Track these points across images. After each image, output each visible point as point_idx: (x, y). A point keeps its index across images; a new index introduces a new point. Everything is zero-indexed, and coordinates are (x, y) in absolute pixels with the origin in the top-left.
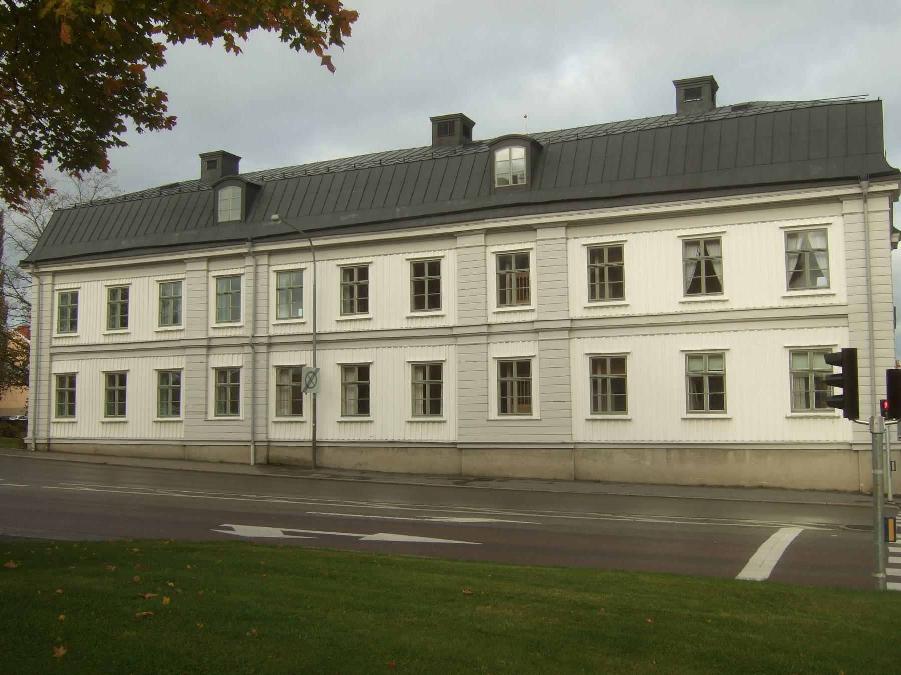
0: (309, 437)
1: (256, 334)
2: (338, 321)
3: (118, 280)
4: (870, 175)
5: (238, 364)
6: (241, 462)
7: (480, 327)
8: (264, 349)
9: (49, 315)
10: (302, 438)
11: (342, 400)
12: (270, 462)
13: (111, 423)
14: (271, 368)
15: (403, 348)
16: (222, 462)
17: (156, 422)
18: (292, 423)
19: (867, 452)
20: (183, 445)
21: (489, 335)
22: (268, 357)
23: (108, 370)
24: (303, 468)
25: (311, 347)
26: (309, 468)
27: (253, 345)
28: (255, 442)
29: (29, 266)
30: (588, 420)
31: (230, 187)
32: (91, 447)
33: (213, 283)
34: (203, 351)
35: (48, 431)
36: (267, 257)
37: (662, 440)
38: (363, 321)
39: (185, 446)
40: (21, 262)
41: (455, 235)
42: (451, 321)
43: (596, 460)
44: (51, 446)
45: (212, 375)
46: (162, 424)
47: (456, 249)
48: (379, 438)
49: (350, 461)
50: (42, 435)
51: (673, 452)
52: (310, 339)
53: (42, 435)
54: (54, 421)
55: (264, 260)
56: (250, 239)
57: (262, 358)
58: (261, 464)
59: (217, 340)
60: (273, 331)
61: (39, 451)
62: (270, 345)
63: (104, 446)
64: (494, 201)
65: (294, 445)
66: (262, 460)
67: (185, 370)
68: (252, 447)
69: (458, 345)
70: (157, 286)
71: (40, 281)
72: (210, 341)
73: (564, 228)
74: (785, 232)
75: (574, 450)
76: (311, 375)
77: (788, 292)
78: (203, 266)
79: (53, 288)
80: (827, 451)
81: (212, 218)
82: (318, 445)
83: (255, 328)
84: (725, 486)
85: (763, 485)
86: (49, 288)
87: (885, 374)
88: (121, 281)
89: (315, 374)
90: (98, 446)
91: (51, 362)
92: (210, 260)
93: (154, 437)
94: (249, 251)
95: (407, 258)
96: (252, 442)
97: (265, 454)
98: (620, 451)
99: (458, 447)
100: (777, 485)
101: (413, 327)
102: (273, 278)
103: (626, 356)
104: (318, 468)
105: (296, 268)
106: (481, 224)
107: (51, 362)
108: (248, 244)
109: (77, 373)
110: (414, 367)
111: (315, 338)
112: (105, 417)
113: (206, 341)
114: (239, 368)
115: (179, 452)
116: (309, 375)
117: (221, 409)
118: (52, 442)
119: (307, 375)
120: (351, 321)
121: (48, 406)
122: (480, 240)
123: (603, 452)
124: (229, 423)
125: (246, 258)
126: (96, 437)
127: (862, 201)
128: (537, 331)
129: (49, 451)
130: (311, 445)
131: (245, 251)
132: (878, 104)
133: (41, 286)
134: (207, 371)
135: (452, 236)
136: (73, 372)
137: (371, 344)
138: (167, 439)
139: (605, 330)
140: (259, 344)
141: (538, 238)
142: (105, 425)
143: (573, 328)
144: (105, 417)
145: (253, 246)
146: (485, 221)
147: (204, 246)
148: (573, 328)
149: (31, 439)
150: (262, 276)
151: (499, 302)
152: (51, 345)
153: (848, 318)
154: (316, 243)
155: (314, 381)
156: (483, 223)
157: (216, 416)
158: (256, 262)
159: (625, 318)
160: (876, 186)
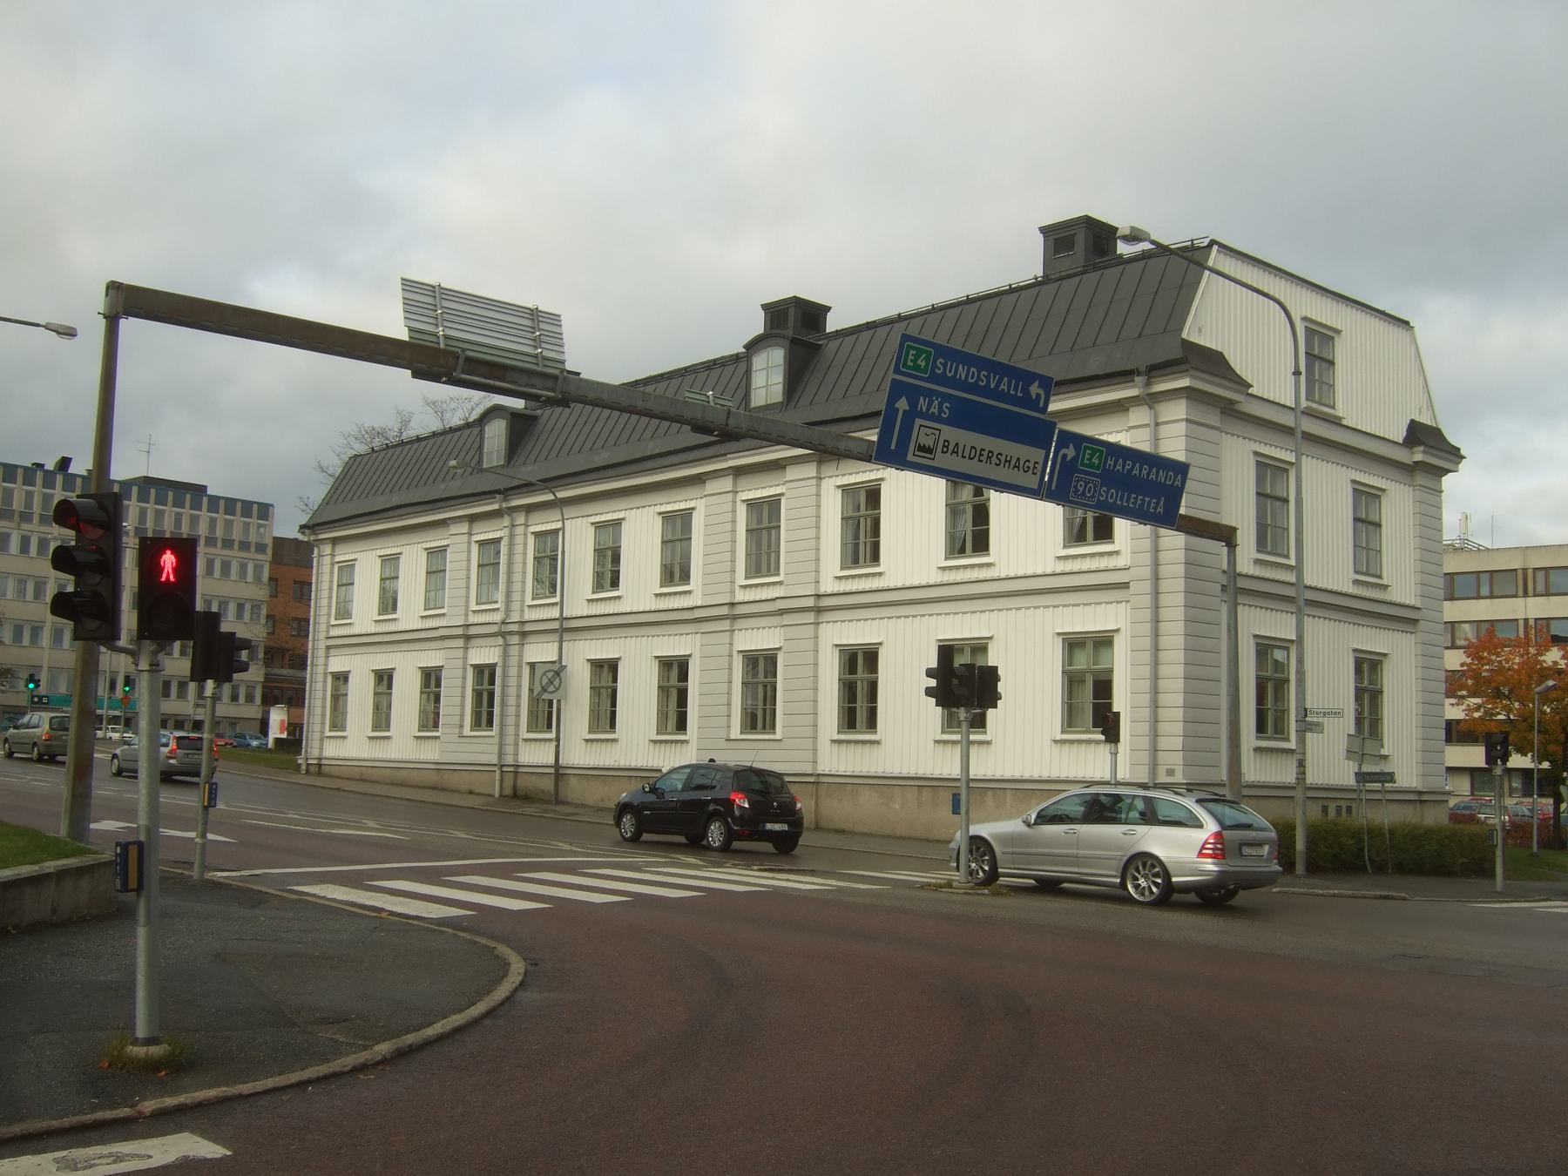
0: (551, 761)
2: (589, 601)
3: (675, 502)
8: (515, 639)
10: (545, 763)
11: (591, 711)
14: (735, 654)
16: (471, 792)
17: (655, 742)
20: (439, 768)
21: (735, 618)
22: (731, 638)
23: (477, 663)
25: (556, 637)
26: (549, 802)
28: (502, 766)
29: (1133, 381)
32: (357, 769)
35: (321, 748)
36: (524, 513)
37: (912, 773)
38: (1079, 559)
40: (302, 527)
42: (696, 600)
44: (323, 767)
47: (706, 496)
48: (623, 763)
50: (315, 753)
51: (925, 789)
52: (556, 625)
55: (520, 519)
56: (1143, 369)
57: (514, 651)
58: (506, 796)
60: (530, 615)
62: (524, 634)
63: (362, 768)
65: (536, 771)
68: (498, 773)
69: (702, 633)
70: (659, 520)
73: (815, 463)
76: (550, 675)
83: (508, 611)
86: (327, 560)
89: (557, 674)
92: (473, 519)
93: (545, 762)
98: (868, 787)
102: (531, 540)
103: (1113, 636)
104: (559, 802)
106: (721, 461)
107: (327, 657)
108: (1138, 379)
109: (690, 656)
114: (494, 665)
115: (432, 778)
117: (477, 724)
118: (324, 762)
119: (544, 674)
120: (544, 605)
122: (726, 483)
123: (849, 788)
125: (1131, 409)
126: (650, 765)
127: (1146, 408)
128: (782, 612)
129: (320, 774)
130: (552, 771)
131: (496, 506)
134: (730, 656)
135: (699, 480)
137: (635, 631)
138: (991, 778)
140: (511, 633)
142: (590, 743)
143: (820, 608)
145: (1148, 384)
146: (729, 456)
148: (820, 608)
150: (519, 539)
153: (1128, 587)
154: (562, 494)
155: (556, 683)
156: (727, 460)
160: (1163, 381)
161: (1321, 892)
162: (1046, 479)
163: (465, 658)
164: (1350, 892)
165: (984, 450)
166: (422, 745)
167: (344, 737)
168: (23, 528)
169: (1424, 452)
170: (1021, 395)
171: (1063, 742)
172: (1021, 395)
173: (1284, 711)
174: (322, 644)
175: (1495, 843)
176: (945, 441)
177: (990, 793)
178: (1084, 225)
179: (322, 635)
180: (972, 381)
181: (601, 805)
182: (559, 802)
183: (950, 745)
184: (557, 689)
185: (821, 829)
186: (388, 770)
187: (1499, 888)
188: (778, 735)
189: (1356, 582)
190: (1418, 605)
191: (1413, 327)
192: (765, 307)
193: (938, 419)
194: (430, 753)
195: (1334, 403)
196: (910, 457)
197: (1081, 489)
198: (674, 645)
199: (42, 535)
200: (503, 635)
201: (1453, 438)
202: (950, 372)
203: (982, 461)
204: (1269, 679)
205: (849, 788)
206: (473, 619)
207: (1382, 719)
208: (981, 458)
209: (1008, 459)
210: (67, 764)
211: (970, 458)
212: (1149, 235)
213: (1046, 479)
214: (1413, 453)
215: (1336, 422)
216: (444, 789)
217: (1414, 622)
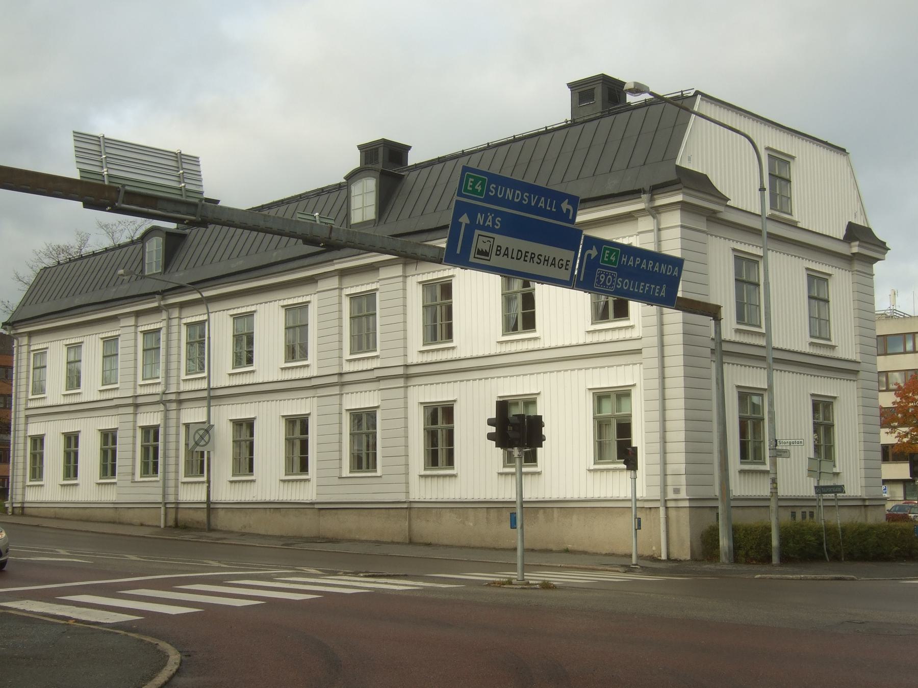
1: (169, 390)
4: (653, 186)
5: (361, 406)
7: (325, 377)
8: (174, 406)
9: (133, 359)
11: (234, 459)
12: (179, 525)
13: (239, 481)
15: (478, 380)
17: (99, 484)
18: (195, 483)
19: (680, 509)
20: (116, 507)
24: (197, 529)
25: (205, 403)
26: (202, 530)
27: (164, 402)
30: (500, 474)
31: (363, 179)
32: (52, 510)
33: (140, 337)
34: (131, 410)
39: (116, 508)
41: (316, 279)
43: (428, 521)
44: (25, 509)
45: (346, 419)
46: (427, 479)
48: (259, 498)
49: (237, 522)
50: (19, 498)
51: (492, 510)
52: (205, 394)
53: (19, 498)
54: (29, 484)
55: (175, 313)
56: (647, 188)
57: (173, 414)
58: (170, 527)
59: (348, 375)
60: (184, 387)
61: (16, 515)
62: (180, 402)
65: (193, 507)
66: (171, 523)
67: (381, 408)
68: (163, 509)
69: (318, 397)
71: (169, 314)
72: (179, 395)
75: (409, 509)
77: (503, 337)
78: (131, 321)
79: (179, 322)
80: (626, 509)
81: (346, 220)
82: (212, 506)
83: (167, 384)
85: (569, 549)
88: (73, 339)
89: (207, 431)
90: (57, 509)
91: (27, 424)
94: (159, 304)
95: (282, 305)
96: (663, 501)
97: (173, 516)
99: (316, 506)
100: (581, 548)
101: (104, 398)
102: (184, 329)
104: (211, 529)
105: (197, 320)
107: (26, 424)
108: (645, 197)
109: (309, 414)
110: (288, 422)
111: (209, 393)
112: (64, 480)
113: (131, 399)
114: (158, 426)
115: (111, 514)
116: (199, 432)
117: (145, 472)
118: (26, 505)
119: (197, 432)
121: (23, 469)
122: (334, 282)
124: (362, 481)
128: (379, 379)
129: (23, 514)
130: (205, 506)
131: (156, 304)
133: (19, 348)
134: (340, 414)
136: (41, 434)
138: (453, 500)
139: (506, 368)
140: (170, 401)
141: (380, 278)
144: (64, 480)
146: (335, 261)
150: (175, 329)
151: (594, 318)
152: (179, 389)
153: (641, 353)
154: (207, 294)
155: (206, 438)
156: (334, 264)
157: (351, 472)
158: (658, 224)
159: (497, 357)
163: (135, 422)
164: (813, 576)
166: (103, 490)
167: (42, 486)
169: (859, 246)
170: (555, 210)
171: (595, 471)
174: (22, 414)
176: (498, 246)
177: (541, 511)
178: (601, 81)
181: (243, 531)
182: (211, 529)
184: (207, 443)
186: (76, 510)
188: (379, 473)
192: (361, 147)
194: (109, 495)
195: (792, 211)
196: (472, 259)
197: (603, 280)
198: (296, 407)
200: (164, 402)
203: (526, 261)
204: (749, 418)
205: (434, 511)
206: (140, 391)
207: (833, 446)
208: (526, 258)
209: (547, 259)
211: (517, 259)
216: (121, 523)
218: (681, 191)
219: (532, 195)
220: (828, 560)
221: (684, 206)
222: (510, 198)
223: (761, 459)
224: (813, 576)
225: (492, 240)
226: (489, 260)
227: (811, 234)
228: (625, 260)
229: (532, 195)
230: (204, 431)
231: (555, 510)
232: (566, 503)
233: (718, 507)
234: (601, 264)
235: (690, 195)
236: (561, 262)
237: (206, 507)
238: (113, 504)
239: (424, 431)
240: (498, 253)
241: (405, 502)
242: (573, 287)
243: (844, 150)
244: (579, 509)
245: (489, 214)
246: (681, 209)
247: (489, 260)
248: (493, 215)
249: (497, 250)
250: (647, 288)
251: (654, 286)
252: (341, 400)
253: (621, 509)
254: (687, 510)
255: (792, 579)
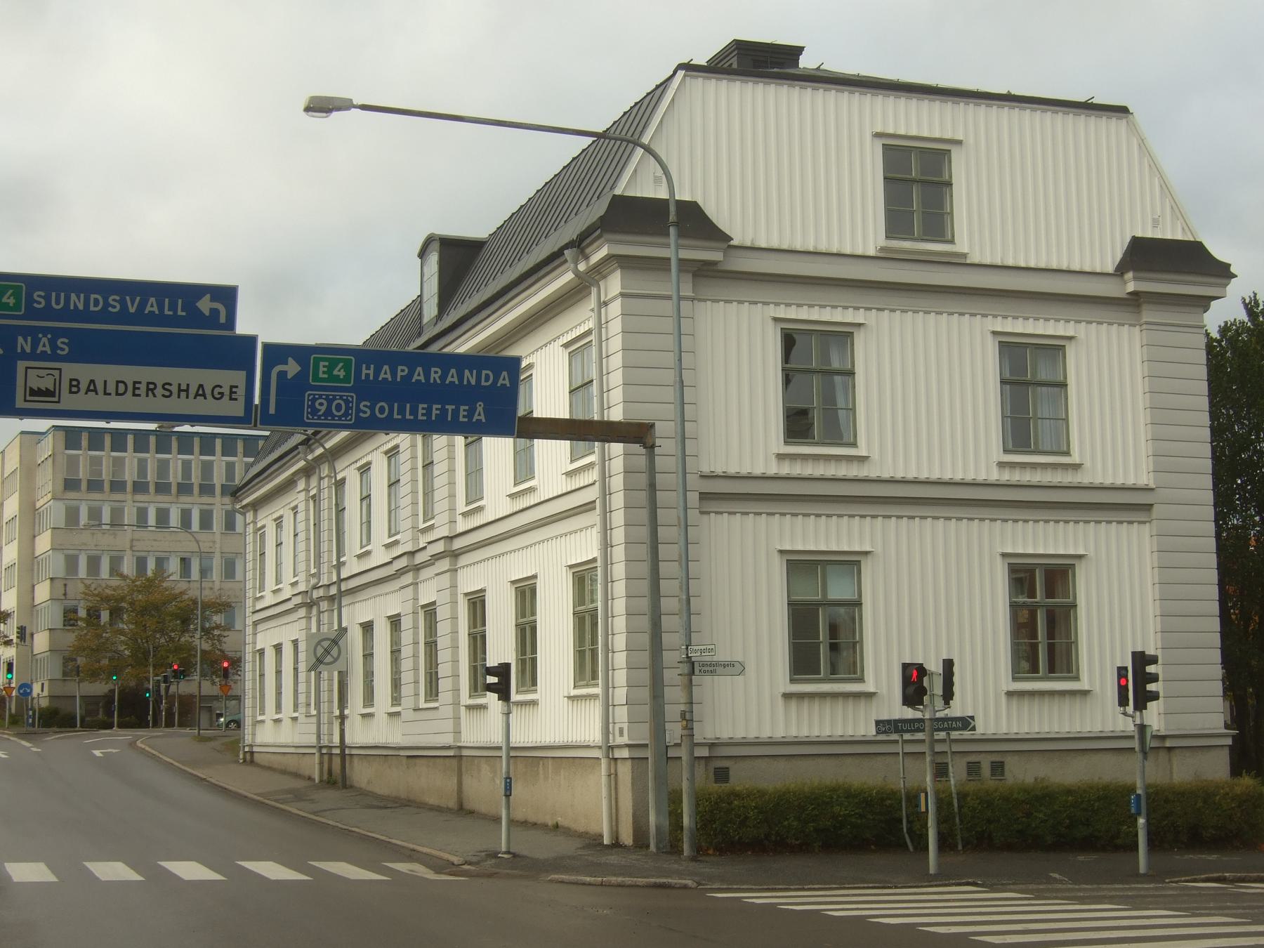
6: (619, 774)
13: (1032, 694)
35: (254, 734)
44: (255, 755)
64: (178, 434)
68: (317, 755)
74: (999, 342)
84: (262, 764)
87: (509, 662)
89: (335, 642)
107: (255, 634)
118: (255, 749)
132: (287, 371)
142: (793, 704)
147: (659, 103)
149: (600, 747)
155: (335, 652)
161: (588, 879)
162: (257, 401)
164: (620, 879)
165: (140, 383)
168: (181, 501)
169: (1135, 279)
170: (184, 314)
172: (184, 314)
173: (855, 644)
174: (249, 621)
175: (923, 809)
176: (71, 380)
178: (736, 52)
179: (249, 610)
180: (59, 307)
183: (841, 699)
184: (336, 660)
185: (472, 812)
187: (932, 869)
189: (1002, 465)
190: (1152, 485)
191: (1132, 113)
193: (54, 357)
195: (953, 236)
196: (20, 403)
197: (323, 409)
199: (205, 507)
201: (1218, 251)
202: (58, 303)
203: (139, 395)
207: (1076, 642)
208: (137, 392)
209: (184, 387)
210: (649, 746)
211: (117, 394)
212: (351, 100)
213: (257, 401)
214: (1125, 283)
215: (958, 262)
217: (1148, 507)
218: (603, 239)
219: (128, 298)
220: (911, 848)
221: (626, 263)
222: (81, 307)
223: (855, 673)
224: (620, 879)
225: (56, 373)
226: (59, 402)
227: (982, 270)
228: (371, 372)
229: (128, 298)
230: (329, 642)
231: (550, 761)
232: (564, 750)
233: (681, 757)
234: (313, 383)
235: (621, 242)
236: (217, 390)
237: (339, 752)
238: (293, 748)
239: (469, 637)
240: (74, 389)
241: (449, 748)
242: (255, 425)
243: (1123, 110)
244: (566, 759)
245: (40, 335)
246: (622, 268)
247: (59, 402)
248: (49, 336)
249: (71, 386)
250: (434, 412)
251: (454, 407)
252: (416, 592)
253: (592, 761)
254: (629, 763)
255: (590, 884)
